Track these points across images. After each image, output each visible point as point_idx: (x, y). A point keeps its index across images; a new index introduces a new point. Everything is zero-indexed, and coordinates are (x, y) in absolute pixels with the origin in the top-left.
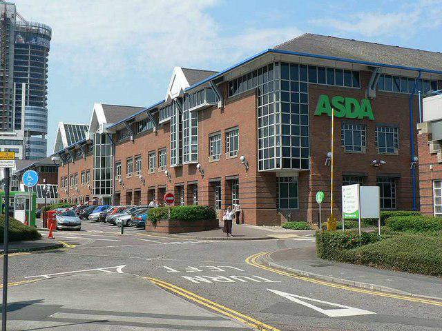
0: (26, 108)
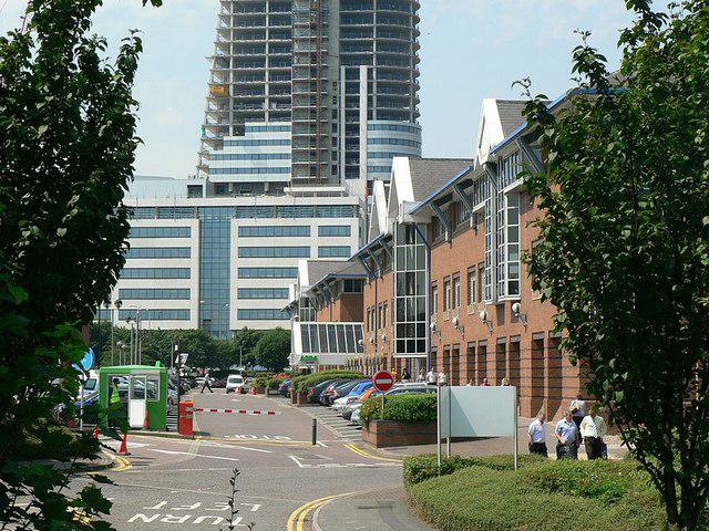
0: (369, 128)
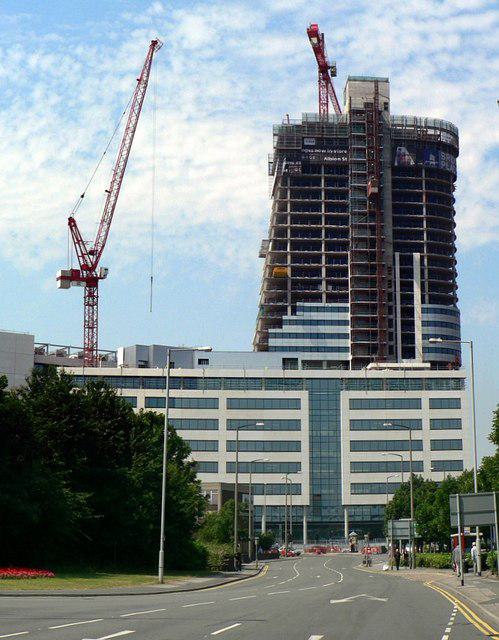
0: (424, 311)
